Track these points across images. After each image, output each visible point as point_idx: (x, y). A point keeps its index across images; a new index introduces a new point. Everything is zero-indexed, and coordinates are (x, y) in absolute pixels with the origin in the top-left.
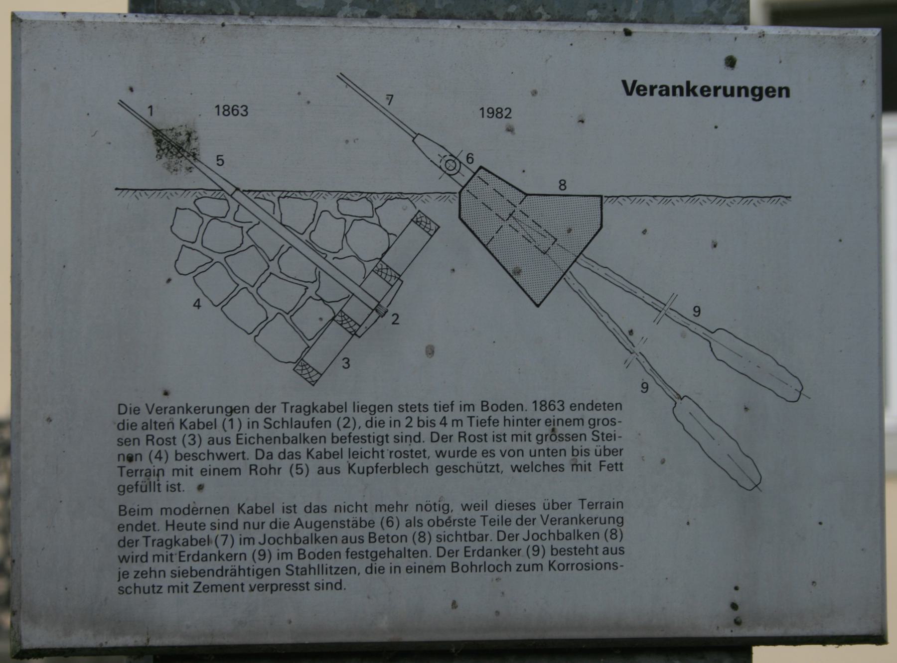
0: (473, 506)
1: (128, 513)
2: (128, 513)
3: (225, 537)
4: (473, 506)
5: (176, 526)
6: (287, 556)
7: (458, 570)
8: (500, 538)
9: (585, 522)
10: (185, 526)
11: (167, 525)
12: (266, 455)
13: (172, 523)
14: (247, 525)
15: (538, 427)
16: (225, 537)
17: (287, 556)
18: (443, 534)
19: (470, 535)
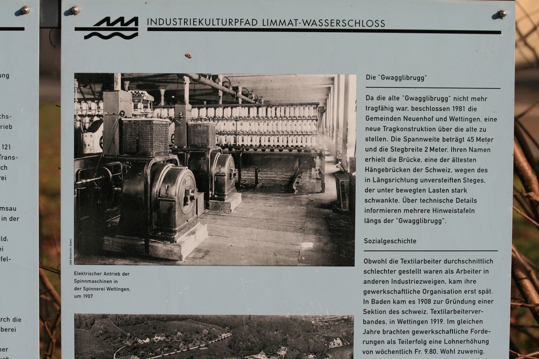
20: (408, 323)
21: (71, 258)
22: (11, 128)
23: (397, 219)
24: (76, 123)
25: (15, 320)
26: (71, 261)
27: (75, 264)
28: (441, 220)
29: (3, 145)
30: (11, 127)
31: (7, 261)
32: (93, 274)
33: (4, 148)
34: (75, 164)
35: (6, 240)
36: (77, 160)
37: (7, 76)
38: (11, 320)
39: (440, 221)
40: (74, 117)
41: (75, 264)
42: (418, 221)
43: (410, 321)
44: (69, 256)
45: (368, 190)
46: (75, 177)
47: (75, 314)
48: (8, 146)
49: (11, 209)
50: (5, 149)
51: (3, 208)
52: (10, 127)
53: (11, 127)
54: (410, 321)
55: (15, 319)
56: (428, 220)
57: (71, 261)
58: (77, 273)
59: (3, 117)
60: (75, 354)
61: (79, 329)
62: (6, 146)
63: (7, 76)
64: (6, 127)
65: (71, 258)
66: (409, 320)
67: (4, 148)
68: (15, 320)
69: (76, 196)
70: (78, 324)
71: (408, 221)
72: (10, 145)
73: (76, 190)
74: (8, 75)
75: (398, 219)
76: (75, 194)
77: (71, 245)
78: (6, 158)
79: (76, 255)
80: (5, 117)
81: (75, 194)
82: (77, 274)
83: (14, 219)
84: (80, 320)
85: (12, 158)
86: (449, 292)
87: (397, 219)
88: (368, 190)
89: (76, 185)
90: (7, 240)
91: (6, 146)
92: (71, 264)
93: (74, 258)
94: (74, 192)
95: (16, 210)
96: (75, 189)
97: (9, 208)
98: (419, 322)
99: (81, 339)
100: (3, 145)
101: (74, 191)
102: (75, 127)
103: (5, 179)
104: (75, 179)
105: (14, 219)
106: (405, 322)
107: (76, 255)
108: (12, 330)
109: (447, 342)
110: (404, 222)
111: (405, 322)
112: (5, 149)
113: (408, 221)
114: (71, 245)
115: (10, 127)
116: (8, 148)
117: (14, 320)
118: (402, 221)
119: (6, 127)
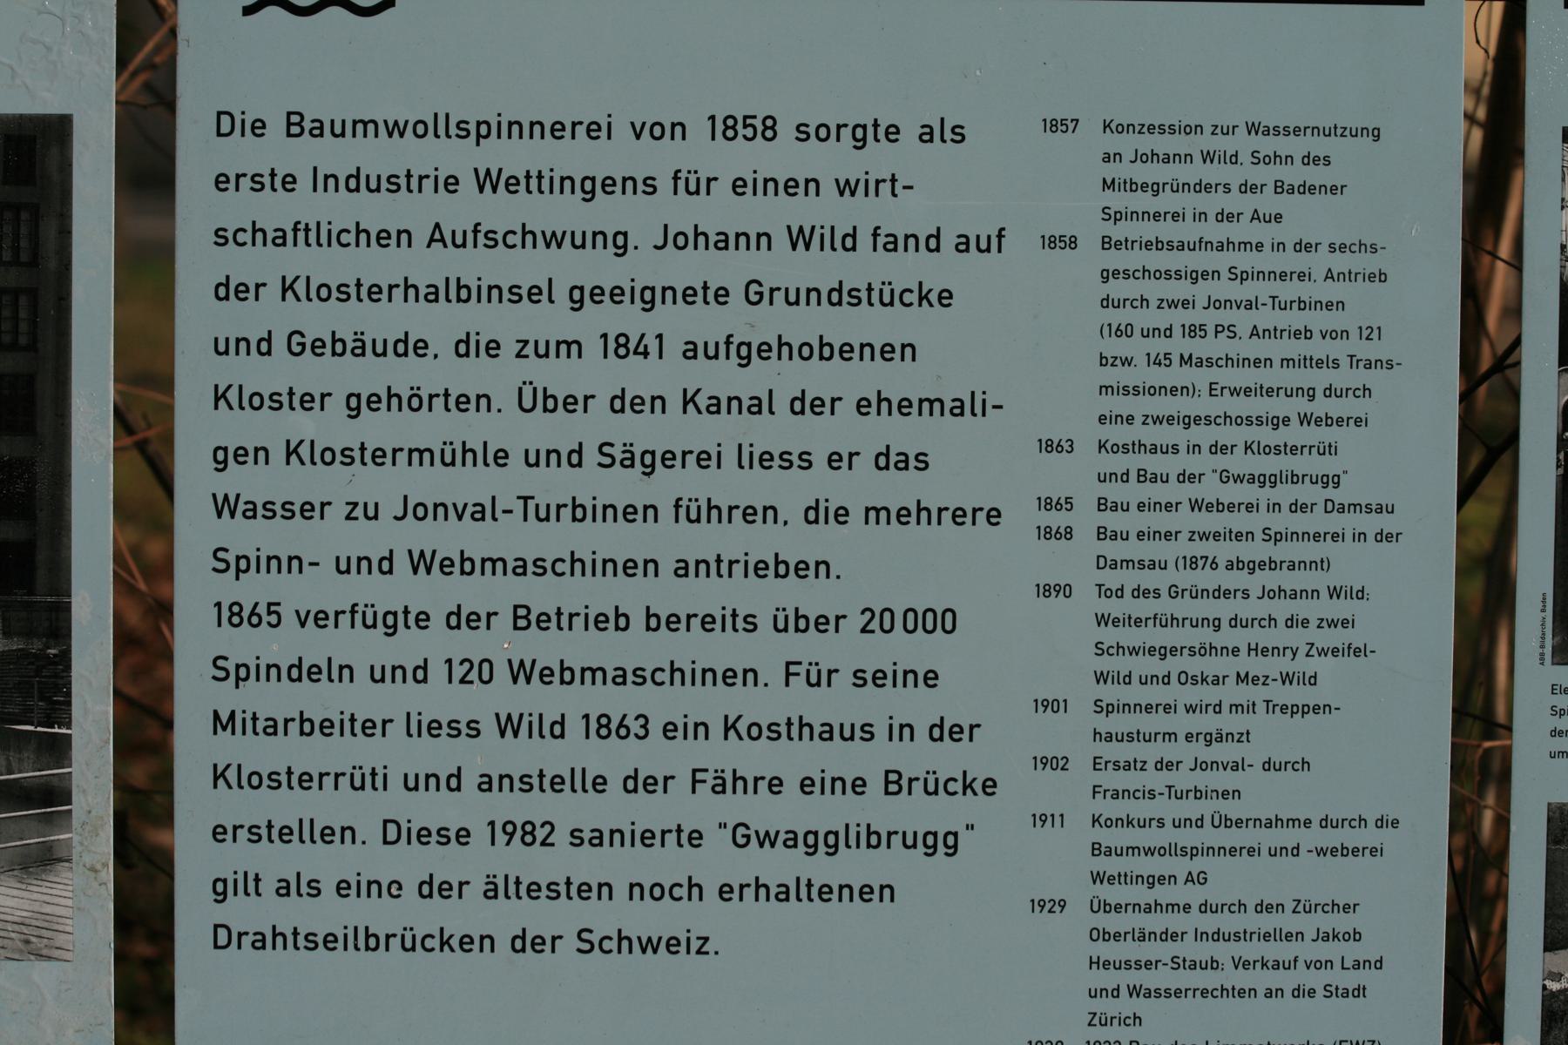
0: (1329, 850)
1: (1113, 246)
2: (1113, 246)
3: (1297, 910)
4: (1329, 850)
5: (1101, 963)
6: (1294, 824)
7: (1051, 508)
8: (1328, 510)
9: (1341, 938)
10: (1112, 964)
11: (1091, 963)
12: (1109, 563)
13: (1093, 965)
14: (637, 890)
15: (1146, 629)
16: (1297, 910)
17: (1294, 824)
18: (1177, 124)
19: (1131, 184)
20: (1120, 883)
21: (1542, 647)
22: (1385, 281)
23: (1214, 471)
24: (1565, 267)
25: (1381, 823)
26: (1542, 654)
27: (1553, 664)
28: (1339, 476)
29: (1360, 328)
30: (1383, 278)
31: (1366, 656)
32: (659, 677)
33: (1364, 336)
34: (1561, 380)
35: (1363, 598)
36: (1563, 370)
37: (1376, 133)
38: (1371, 823)
39: (1336, 479)
40: (1559, 251)
41: (1553, 664)
42: (1273, 479)
43: (1126, 875)
44: (1536, 643)
45: (227, 290)
46: (1561, 418)
47: (1549, 804)
48: (1376, 332)
49: (1380, 510)
50: (1367, 339)
51: (1358, 507)
52: (1382, 277)
53: (1383, 278)
54: (1126, 875)
55: (1382, 820)
56: (1303, 476)
57: (1542, 654)
58: (1558, 687)
59: (1363, 247)
60: (1547, 917)
61: (1558, 847)
62: (1370, 330)
63: (1376, 133)
64: (1371, 277)
65: (1542, 647)
66: (1123, 874)
67: (1364, 336)
68: (1381, 823)
69: (1561, 471)
70: (1557, 832)
71: (1247, 477)
72: (1379, 328)
73: (1562, 456)
74: (1379, 129)
75: (1219, 472)
76: (1558, 467)
77: (1543, 611)
78: (1368, 366)
79: (1556, 639)
80: (1369, 249)
81: (1558, 467)
82: (1558, 691)
83: (1389, 538)
84: (1561, 822)
85: (1385, 365)
86: (1129, 766)
87: (1214, 471)
88: (227, 290)
89: (1563, 440)
90: (1366, 596)
91: (1370, 330)
92: (1542, 664)
93: (1553, 648)
94: (1555, 460)
95: (1392, 512)
96: (1558, 452)
97: (1374, 507)
98: (1151, 880)
99: (1563, 874)
100: (1360, 328)
101: (1558, 458)
102: (1561, 279)
103: (1363, 423)
104: (1561, 425)
105: (1389, 538)
106: (1111, 880)
107: (1556, 639)
108: (1373, 852)
109: (1348, 964)
110: (1235, 482)
111: (1111, 880)
112: (1367, 339)
113: (1247, 477)
114: (1543, 611)
115: (1382, 277)
116: (1375, 335)
117: (1379, 823)
118: (1228, 477)
119: (1371, 277)
